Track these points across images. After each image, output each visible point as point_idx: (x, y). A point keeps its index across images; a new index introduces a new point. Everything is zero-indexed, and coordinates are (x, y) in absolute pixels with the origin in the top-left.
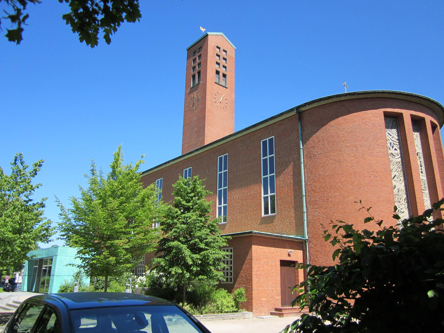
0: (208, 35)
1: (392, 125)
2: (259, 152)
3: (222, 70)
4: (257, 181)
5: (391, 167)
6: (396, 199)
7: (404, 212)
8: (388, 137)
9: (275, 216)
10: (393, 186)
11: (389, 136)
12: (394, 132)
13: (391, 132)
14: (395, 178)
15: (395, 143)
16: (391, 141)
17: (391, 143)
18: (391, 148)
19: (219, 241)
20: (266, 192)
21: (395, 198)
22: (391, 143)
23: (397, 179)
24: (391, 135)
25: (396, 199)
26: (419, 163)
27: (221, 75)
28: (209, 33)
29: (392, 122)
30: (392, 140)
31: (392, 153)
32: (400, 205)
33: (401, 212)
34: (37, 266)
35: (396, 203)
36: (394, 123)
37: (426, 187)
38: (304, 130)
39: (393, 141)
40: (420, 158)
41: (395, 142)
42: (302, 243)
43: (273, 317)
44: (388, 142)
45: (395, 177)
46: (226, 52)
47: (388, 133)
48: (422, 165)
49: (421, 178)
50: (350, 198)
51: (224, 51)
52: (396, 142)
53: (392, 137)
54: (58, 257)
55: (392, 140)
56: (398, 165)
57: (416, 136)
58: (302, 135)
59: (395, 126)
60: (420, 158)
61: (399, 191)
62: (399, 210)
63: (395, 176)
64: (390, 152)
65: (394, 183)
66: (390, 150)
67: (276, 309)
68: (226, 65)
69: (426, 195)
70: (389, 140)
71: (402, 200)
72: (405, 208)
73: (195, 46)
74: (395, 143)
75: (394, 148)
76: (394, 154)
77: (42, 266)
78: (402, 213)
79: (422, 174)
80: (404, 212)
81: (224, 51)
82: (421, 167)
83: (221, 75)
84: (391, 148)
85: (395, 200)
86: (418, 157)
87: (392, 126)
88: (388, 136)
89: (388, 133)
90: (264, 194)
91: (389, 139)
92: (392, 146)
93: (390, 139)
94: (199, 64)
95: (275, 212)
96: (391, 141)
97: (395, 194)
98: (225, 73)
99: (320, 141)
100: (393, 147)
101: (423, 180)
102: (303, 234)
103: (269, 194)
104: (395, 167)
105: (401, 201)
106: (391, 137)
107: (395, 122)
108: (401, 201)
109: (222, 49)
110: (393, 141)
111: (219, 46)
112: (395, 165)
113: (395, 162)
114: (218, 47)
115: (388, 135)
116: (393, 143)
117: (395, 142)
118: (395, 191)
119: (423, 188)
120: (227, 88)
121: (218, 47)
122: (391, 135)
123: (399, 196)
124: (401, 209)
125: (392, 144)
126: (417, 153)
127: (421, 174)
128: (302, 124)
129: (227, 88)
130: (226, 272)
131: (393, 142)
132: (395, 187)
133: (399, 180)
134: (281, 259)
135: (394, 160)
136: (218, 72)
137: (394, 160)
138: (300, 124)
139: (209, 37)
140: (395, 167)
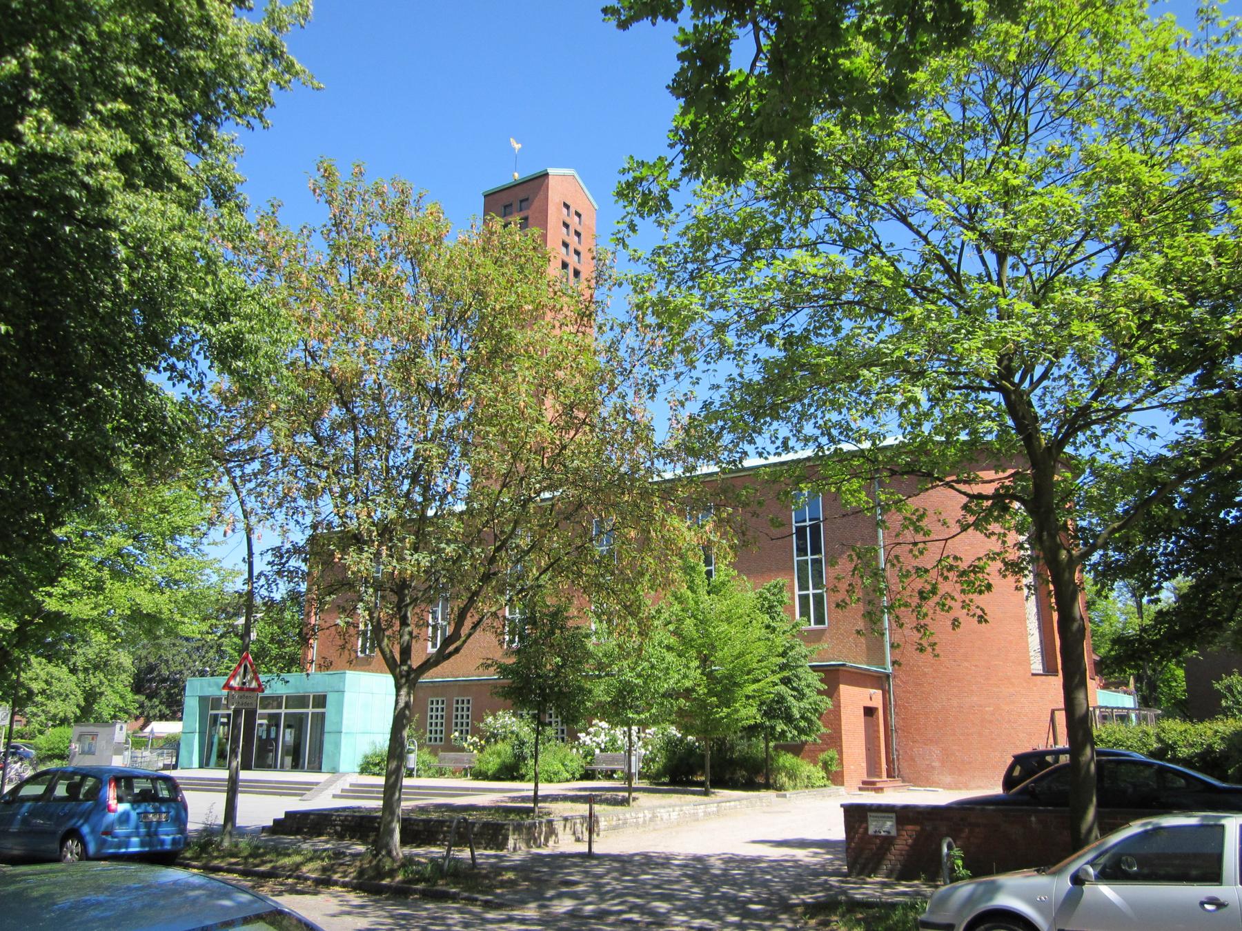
0: (547, 175)
3: (573, 260)
4: (786, 568)
9: (823, 631)
19: (408, 629)
20: (803, 586)
28: (550, 171)
42: (879, 678)
43: (739, 800)
46: (578, 215)
54: (346, 694)
67: (864, 783)
68: (579, 248)
90: (800, 589)
95: (823, 623)
98: (578, 268)
102: (882, 662)
103: (811, 591)
109: (572, 210)
114: (567, 206)
136: (565, 265)
139: (552, 182)
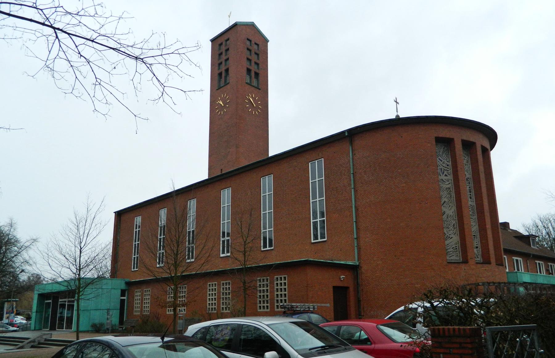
1: (444, 150)
2: (307, 175)
5: (441, 193)
6: (445, 225)
7: (452, 238)
8: (440, 163)
10: (443, 212)
11: (440, 162)
12: (445, 158)
13: (442, 158)
14: (445, 205)
15: (445, 169)
16: (442, 167)
17: (441, 169)
18: (441, 174)
21: (444, 224)
22: (441, 169)
23: (446, 206)
24: (442, 161)
25: (445, 225)
26: (468, 188)
27: (253, 74)
29: (443, 147)
30: (442, 166)
31: (442, 180)
32: (449, 231)
33: (450, 237)
34: (50, 301)
35: (445, 229)
36: (446, 148)
37: (474, 213)
38: (355, 154)
39: (444, 167)
40: (469, 184)
41: (445, 167)
44: (438, 168)
45: (444, 204)
46: (258, 45)
47: (439, 159)
48: (471, 190)
49: (469, 204)
50: (401, 224)
51: (256, 44)
52: (446, 168)
53: (443, 163)
55: (442, 166)
56: (448, 191)
57: (296, 312)
58: (353, 159)
59: (446, 152)
60: (469, 184)
61: (448, 217)
62: (448, 236)
63: (445, 202)
64: (440, 178)
65: (444, 209)
66: (440, 176)
69: (473, 221)
70: (440, 166)
71: (450, 226)
72: (454, 234)
73: (221, 37)
74: (445, 169)
75: (444, 174)
76: (444, 180)
77: (59, 300)
78: (451, 239)
79: (471, 200)
80: (452, 238)
81: (256, 44)
82: (470, 192)
83: (253, 74)
84: (441, 174)
85: (444, 226)
86: (467, 182)
87: (443, 152)
88: (439, 162)
89: (439, 159)
91: (440, 164)
92: (442, 172)
93: (441, 164)
94: (227, 60)
96: (442, 167)
97: (444, 220)
98: (257, 71)
99: (371, 166)
100: (443, 173)
101: (471, 205)
104: (445, 194)
105: (450, 227)
106: (441, 163)
107: (446, 147)
108: (450, 227)
109: (253, 42)
110: (444, 167)
111: (250, 39)
112: (444, 192)
113: (445, 188)
115: (439, 160)
116: (444, 169)
117: (445, 167)
118: (445, 217)
119: (472, 214)
120: (260, 89)
121: (248, 39)
122: (442, 161)
123: (448, 222)
124: (450, 235)
125: (443, 170)
126: (466, 178)
127: (470, 199)
128: (353, 148)
129: (260, 89)
130: (266, 306)
131: (443, 168)
132: (445, 213)
133: (448, 206)
134: (334, 285)
135: (444, 187)
136: (249, 71)
137: (444, 186)
138: (351, 148)
140: (445, 194)
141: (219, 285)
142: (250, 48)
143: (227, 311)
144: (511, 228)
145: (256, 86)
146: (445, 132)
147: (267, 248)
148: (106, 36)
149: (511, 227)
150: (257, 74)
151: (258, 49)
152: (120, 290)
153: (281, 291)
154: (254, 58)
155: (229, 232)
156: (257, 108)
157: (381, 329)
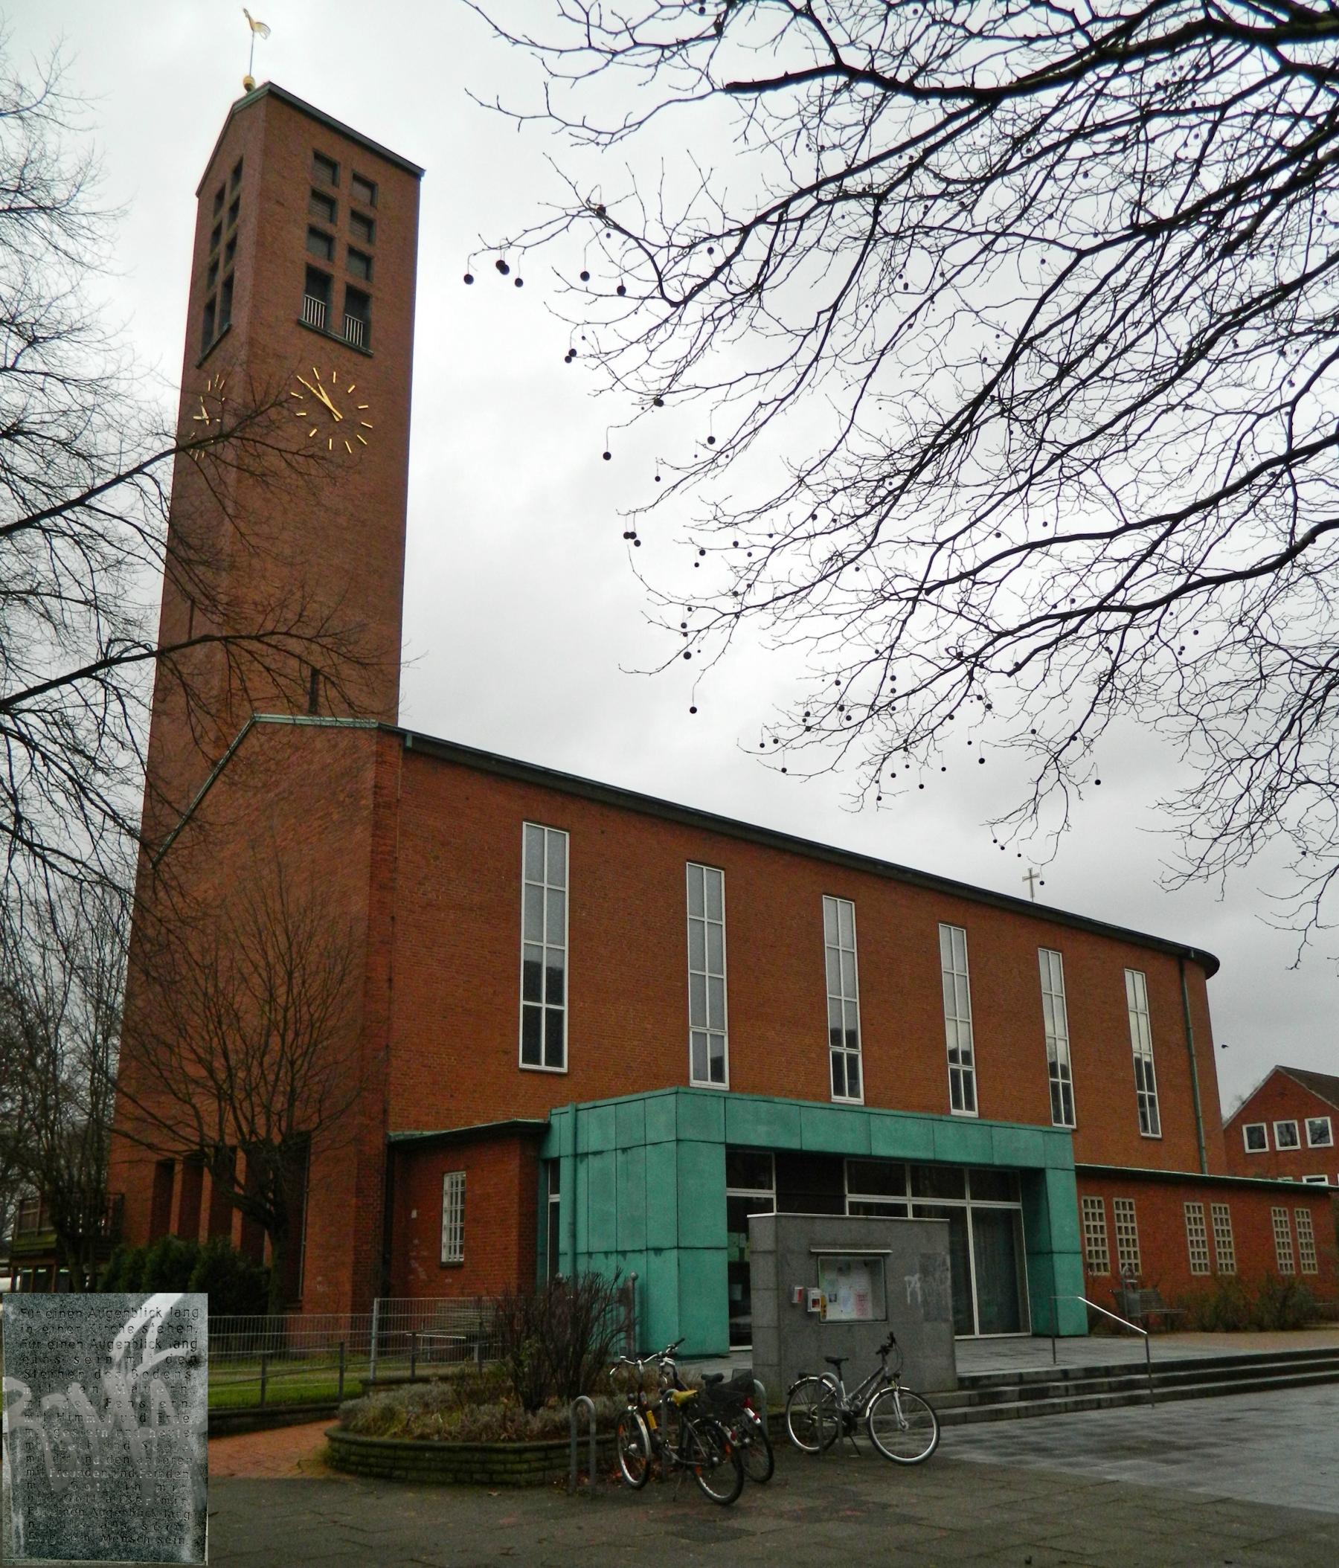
51: (357, 178)
98: (361, 284)
129: (370, 356)
141: (1207, 1210)
142: (327, 189)
143: (1204, 1273)
144: (1208, 981)
145: (359, 343)
146: (337, 150)
147: (562, 1012)
148: (1045, 651)
149: (1210, 983)
150: (357, 300)
151: (372, 203)
152: (722, 1152)
153: (1127, 1233)
154: (345, 232)
155: (558, 965)
156: (350, 425)
157: (310, 1422)
